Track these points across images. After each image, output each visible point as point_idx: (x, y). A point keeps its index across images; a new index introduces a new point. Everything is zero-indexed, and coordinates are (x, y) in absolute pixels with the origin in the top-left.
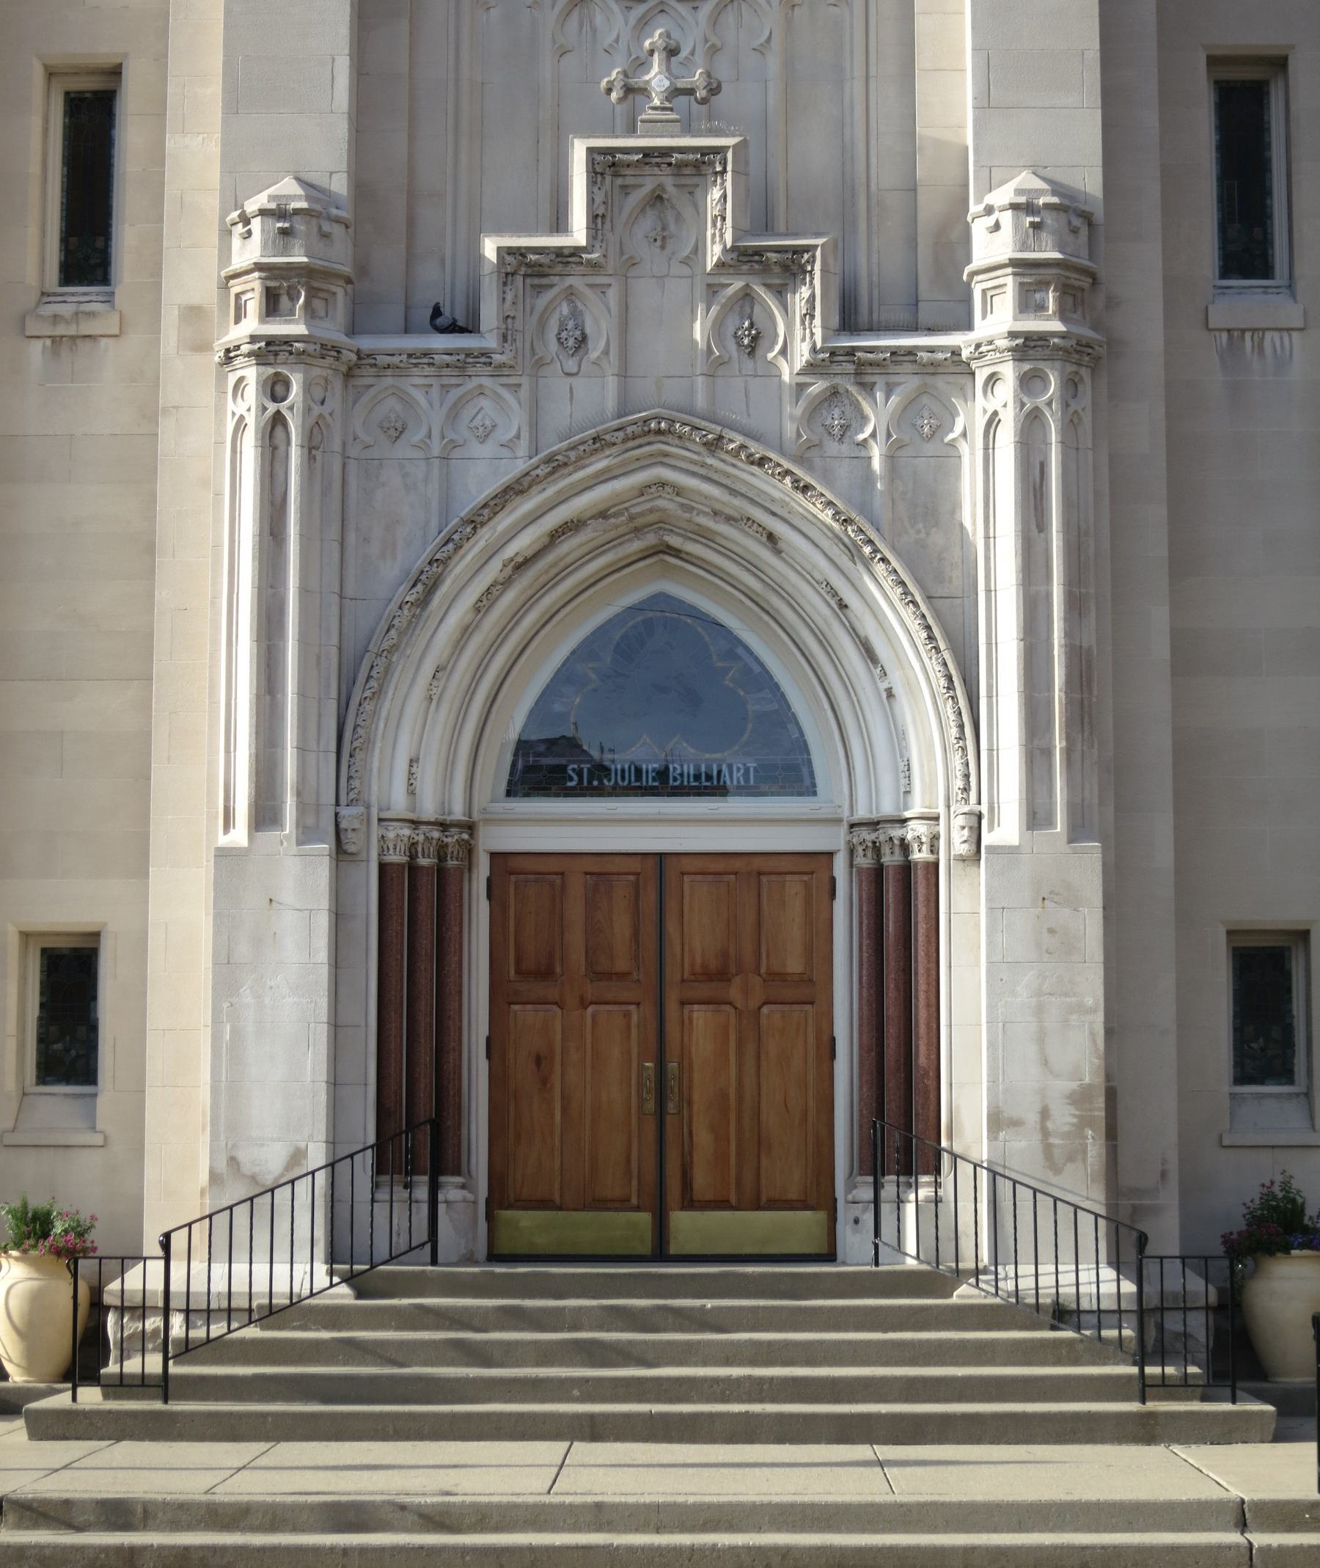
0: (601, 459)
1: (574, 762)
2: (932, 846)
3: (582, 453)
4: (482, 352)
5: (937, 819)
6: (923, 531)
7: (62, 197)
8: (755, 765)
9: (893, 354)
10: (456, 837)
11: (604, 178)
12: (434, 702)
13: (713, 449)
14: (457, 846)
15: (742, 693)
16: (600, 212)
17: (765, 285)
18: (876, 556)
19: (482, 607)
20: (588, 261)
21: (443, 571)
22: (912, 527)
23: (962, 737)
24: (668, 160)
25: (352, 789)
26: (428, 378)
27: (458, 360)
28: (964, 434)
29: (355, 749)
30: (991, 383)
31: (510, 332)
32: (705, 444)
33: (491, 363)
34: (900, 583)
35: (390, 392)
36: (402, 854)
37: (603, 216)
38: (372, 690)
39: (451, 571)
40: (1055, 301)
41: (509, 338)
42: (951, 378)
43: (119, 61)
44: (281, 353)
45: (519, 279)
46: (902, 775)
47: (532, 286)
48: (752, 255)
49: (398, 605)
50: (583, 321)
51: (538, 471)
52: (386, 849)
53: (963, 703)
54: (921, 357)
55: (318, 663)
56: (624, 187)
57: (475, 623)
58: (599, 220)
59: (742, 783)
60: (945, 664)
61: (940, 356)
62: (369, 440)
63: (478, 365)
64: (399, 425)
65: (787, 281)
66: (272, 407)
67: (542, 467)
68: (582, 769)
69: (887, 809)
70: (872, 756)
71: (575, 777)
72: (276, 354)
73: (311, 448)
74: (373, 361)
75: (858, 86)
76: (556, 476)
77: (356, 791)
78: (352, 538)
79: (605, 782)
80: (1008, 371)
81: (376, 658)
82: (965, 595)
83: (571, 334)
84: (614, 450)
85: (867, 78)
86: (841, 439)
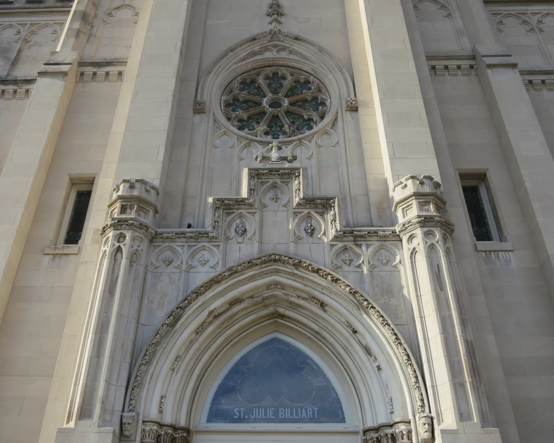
0: (251, 271)
1: (237, 407)
2: (408, 436)
3: (243, 267)
4: (205, 232)
5: (409, 422)
6: (387, 299)
7: (70, 220)
8: (317, 409)
9: (369, 233)
10: (180, 435)
11: (254, 179)
12: (175, 372)
13: (297, 267)
14: (181, 440)
15: (310, 378)
16: (253, 188)
17: (316, 212)
18: (369, 306)
19: (198, 331)
20: (248, 203)
21: (182, 313)
22: (382, 297)
23: (418, 382)
24: (278, 173)
25: (131, 405)
26: (183, 243)
27: (195, 235)
28: (400, 262)
29: (135, 386)
30: (411, 239)
31: (216, 227)
32: (294, 265)
33: (208, 237)
34: (381, 316)
35: (168, 248)
36: (153, 439)
37: (254, 190)
38: (146, 360)
39: (186, 313)
40: (433, 207)
41: (216, 228)
42: (392, 242)
43: (93, 176)
44: (124, 225)
45: (221, 210)
46: (388, 405)
47: (226, 213)
48: (311, 201)
49: (162, 324)
50: (245, 225)
51: (225, 274)
52: (145, 436)
53: (415, 366)
54: (380, 233)
55: (122, 347)
56: (262, 183)
57: (196, 339)
58: (252, 191)
59: (312, 417)
60: (405, 350)
61: (388, 233)
62: (157, 265)
63: (203, 238)
64: (170, 260)
65: (324, 211)
66: (117, 245)
67: (227, 272)
68: (241, 410)
69: (382, 420)
70: (372, 400)
71: (238, 414)
72: (121, 225)
73: (131, 262)
74: (162, 236)
75: (344, 166)
76: (232, 277)
77: (133, 406)
78: (145, 301)
79: (251, 416)
80: (419, 232)
81: (149, 347)
82: (409, 323)
83: (240, 228)
84: (257, 267)
85: (347, 164)
86: (349, 265)
